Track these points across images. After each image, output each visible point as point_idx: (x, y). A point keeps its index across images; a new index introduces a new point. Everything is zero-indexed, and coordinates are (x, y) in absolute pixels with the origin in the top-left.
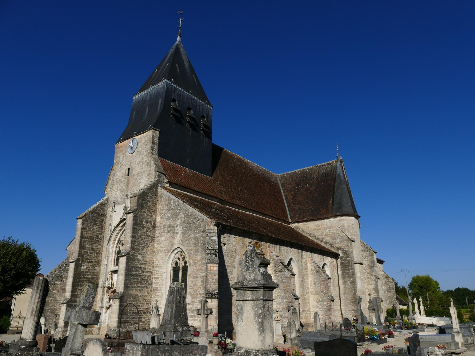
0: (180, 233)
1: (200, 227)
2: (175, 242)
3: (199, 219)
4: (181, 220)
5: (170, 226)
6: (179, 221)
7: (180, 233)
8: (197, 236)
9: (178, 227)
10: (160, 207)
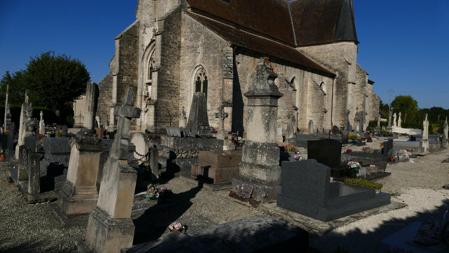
0: (201, 53)
3: (217, 41)
4: (202, 42)
5: (193, 47)
6: (200, 42)
7: (201, 53)
8: (216, 55)
9: (200, 47)
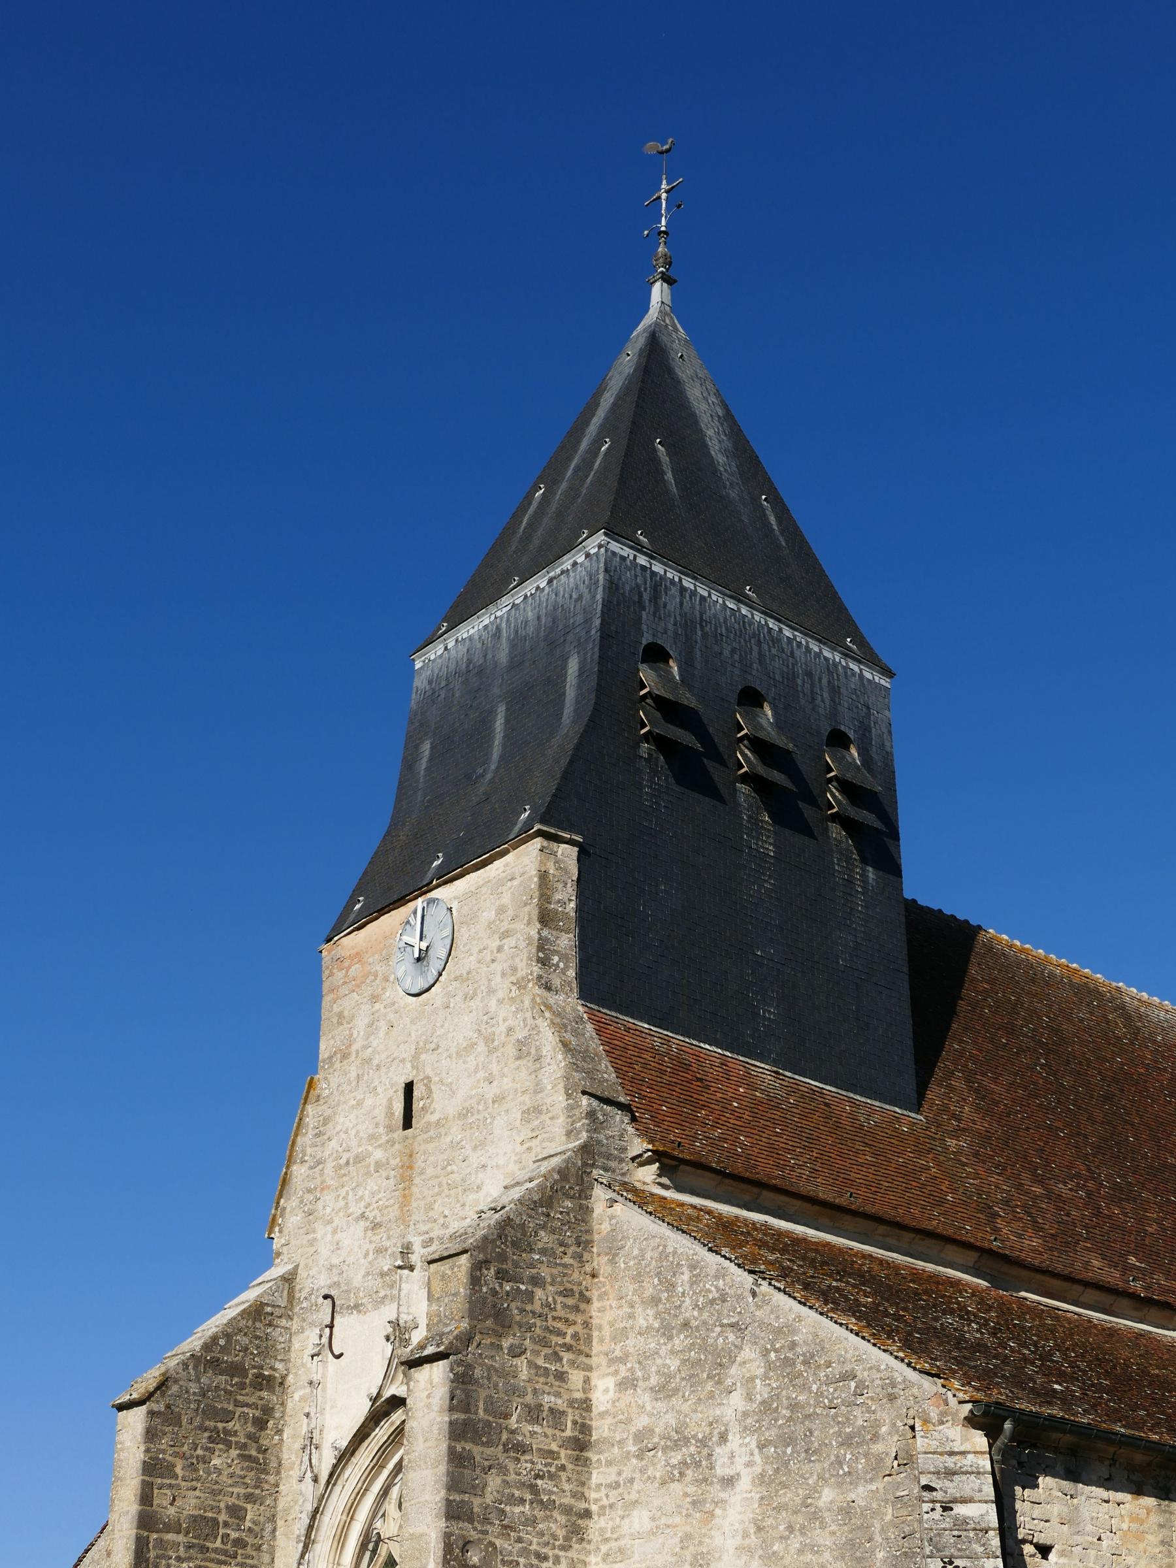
0: (744, 1483)
1: (875, 1438)
2: (718, 1540)
4: (749, 1398)
5: (679, 1439)
6: (737, 1400)
9: (734, 1441)
10: (609, 1316)
